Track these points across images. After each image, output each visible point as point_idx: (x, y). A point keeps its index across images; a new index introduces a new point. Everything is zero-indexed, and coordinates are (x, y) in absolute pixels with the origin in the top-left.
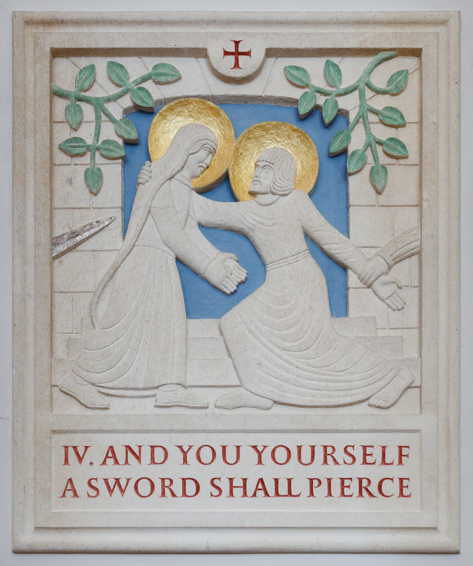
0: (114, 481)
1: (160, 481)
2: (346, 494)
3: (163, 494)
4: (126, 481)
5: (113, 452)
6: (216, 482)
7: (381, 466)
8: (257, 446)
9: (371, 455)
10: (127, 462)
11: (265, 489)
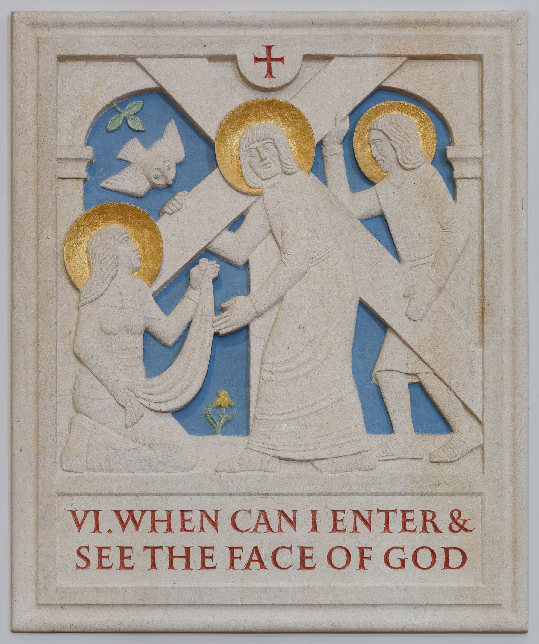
1: (358, 552)
6: (83, 551)
7: (151, 534)
8: (133, 511)
10: (280, 530)
11: (267, 522)
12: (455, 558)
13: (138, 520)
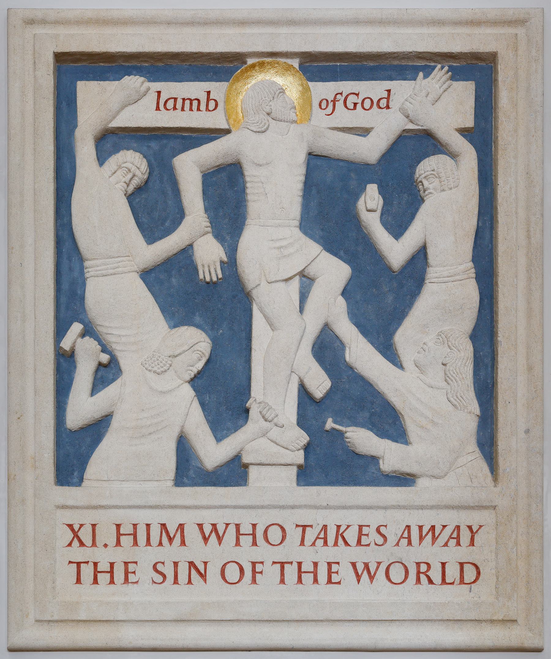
0: (363, 566)
2: (333, 581)
3: (418, 581)
4: (376, 565)
5: (326, 533)
6: (160, 567)
9: (367, 535)
12: (470, 574)
13: (221, 534)
